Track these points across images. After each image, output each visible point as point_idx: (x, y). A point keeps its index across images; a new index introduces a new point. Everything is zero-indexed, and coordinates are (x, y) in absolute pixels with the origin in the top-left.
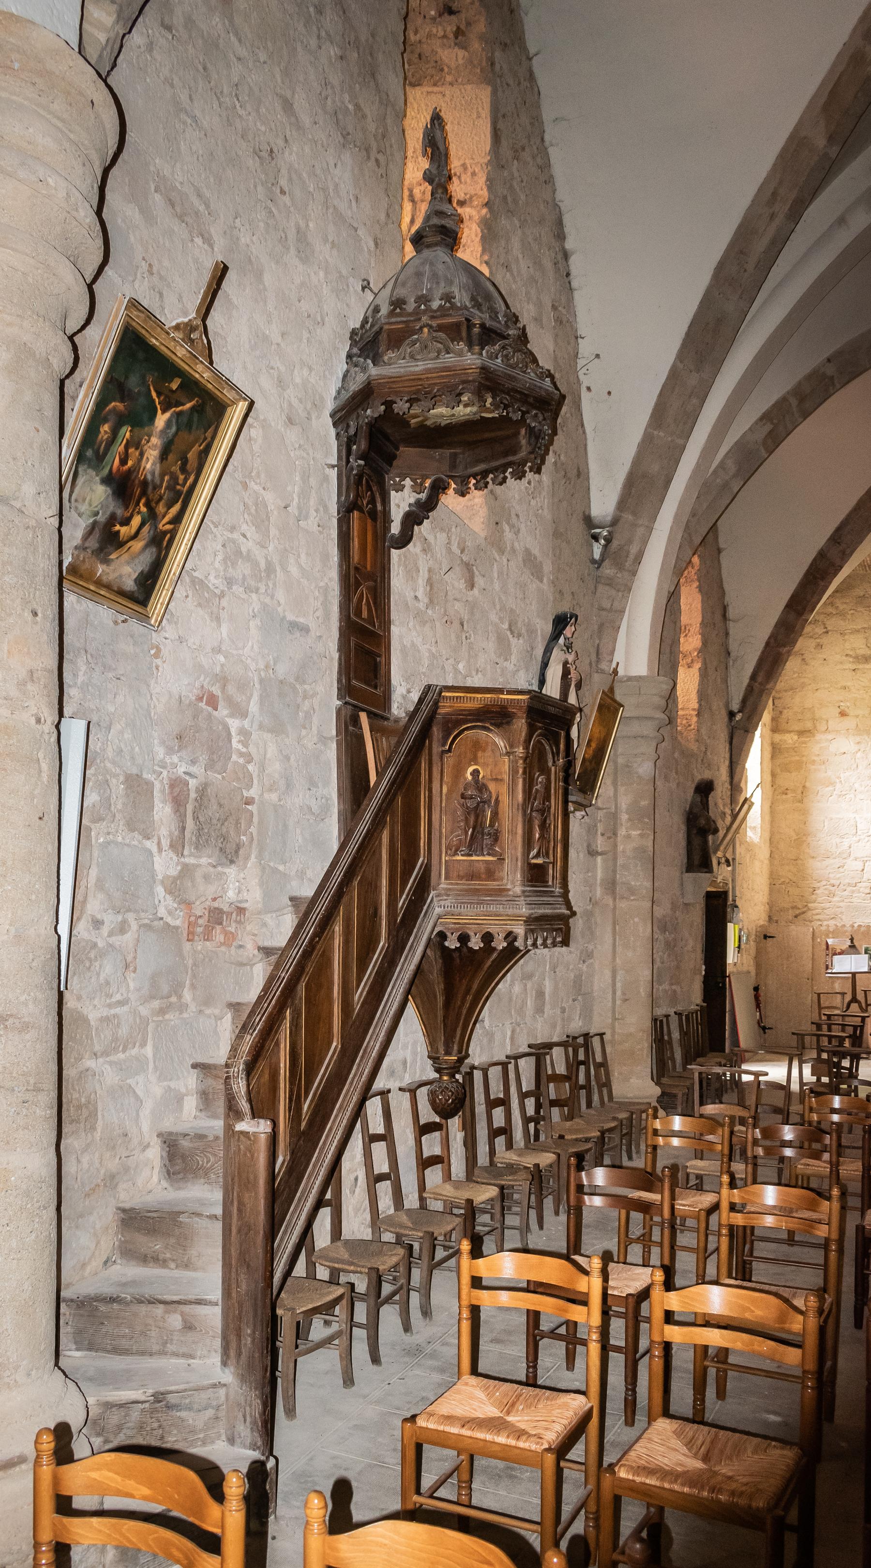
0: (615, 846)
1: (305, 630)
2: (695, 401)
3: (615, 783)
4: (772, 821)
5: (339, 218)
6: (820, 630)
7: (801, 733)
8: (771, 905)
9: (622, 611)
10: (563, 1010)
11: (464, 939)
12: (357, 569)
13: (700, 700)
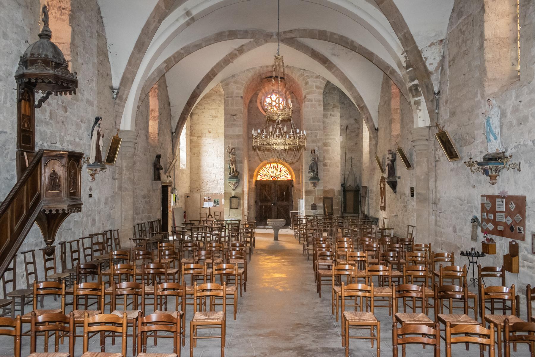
0: (122, 177)
1: (6, 133)
2: (138, 61)
3: (121, 159)
4: (191, 162)
5: (17, 26)
6: (203, 108)
7: (198, 137)
8: (191, 187)
9: (122, 112)
10: (103, 224)
11: (50, 211)
12: (23, 115)
13: (159, 130)
